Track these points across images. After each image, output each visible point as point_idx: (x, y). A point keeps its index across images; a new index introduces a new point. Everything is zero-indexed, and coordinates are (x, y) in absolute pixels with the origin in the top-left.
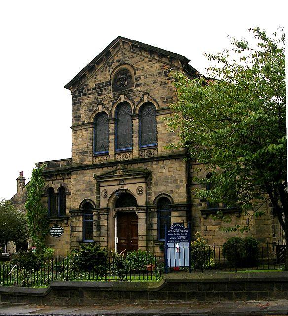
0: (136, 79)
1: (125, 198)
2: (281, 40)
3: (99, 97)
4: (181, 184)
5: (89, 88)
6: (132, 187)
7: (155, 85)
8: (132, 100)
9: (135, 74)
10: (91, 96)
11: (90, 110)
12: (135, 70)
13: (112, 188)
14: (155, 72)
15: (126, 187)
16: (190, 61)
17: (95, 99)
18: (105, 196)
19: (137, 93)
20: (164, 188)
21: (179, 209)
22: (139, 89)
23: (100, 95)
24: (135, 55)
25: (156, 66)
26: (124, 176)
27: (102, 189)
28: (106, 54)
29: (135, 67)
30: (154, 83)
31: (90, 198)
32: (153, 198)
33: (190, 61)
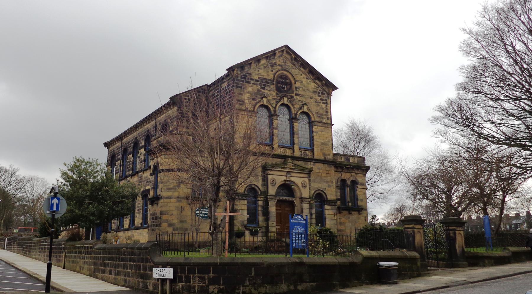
0: (296, 88)
1: (287, 188)
2: (346, 176)
3: (263, 91)
4: (331, 184)
5: (252, 78)
6: (298, 179)
7: (312, 100)
8: (293, 105)
9: (295, 83)
10: (255, 86)
11: (253, 99)
12: (296, 81)
13: (278, 178)
14: (312, 90)
15: (292, 179)
16: (337, 88)
17: (258, 90)
18: (274, 184)
19: (297, 101)
20: (320, 185)
21: (331, 204)
22: (298, 97)
23: (264, 88)
24: (294, 67)
25: (312, 85)
26: (294, 169)
27: (270, 177)
28: (270, 55)
29: (297, 79)
30: (311, 98)
31: (255, 183)
32: (313, 192)
33: (337, 88)
